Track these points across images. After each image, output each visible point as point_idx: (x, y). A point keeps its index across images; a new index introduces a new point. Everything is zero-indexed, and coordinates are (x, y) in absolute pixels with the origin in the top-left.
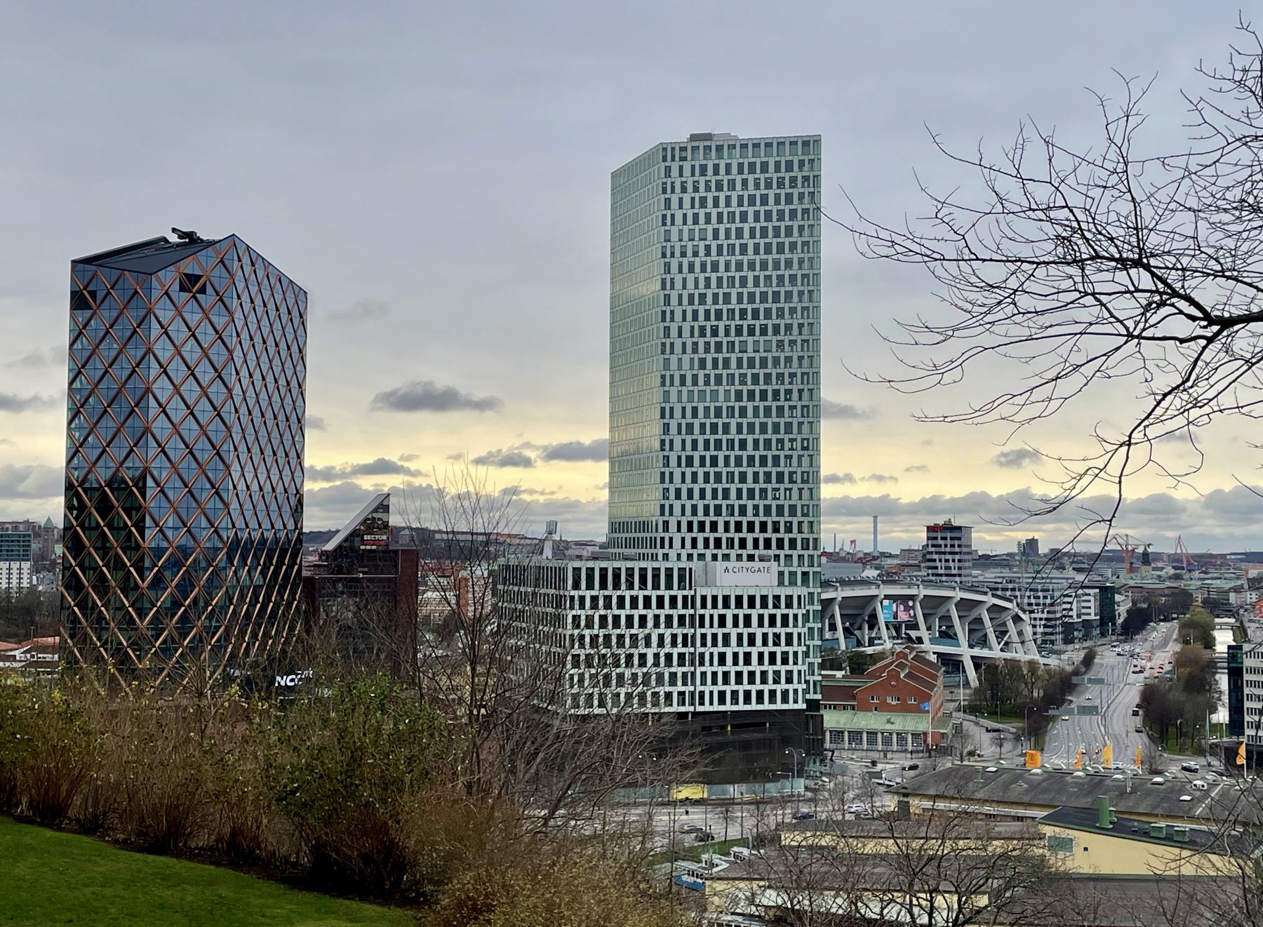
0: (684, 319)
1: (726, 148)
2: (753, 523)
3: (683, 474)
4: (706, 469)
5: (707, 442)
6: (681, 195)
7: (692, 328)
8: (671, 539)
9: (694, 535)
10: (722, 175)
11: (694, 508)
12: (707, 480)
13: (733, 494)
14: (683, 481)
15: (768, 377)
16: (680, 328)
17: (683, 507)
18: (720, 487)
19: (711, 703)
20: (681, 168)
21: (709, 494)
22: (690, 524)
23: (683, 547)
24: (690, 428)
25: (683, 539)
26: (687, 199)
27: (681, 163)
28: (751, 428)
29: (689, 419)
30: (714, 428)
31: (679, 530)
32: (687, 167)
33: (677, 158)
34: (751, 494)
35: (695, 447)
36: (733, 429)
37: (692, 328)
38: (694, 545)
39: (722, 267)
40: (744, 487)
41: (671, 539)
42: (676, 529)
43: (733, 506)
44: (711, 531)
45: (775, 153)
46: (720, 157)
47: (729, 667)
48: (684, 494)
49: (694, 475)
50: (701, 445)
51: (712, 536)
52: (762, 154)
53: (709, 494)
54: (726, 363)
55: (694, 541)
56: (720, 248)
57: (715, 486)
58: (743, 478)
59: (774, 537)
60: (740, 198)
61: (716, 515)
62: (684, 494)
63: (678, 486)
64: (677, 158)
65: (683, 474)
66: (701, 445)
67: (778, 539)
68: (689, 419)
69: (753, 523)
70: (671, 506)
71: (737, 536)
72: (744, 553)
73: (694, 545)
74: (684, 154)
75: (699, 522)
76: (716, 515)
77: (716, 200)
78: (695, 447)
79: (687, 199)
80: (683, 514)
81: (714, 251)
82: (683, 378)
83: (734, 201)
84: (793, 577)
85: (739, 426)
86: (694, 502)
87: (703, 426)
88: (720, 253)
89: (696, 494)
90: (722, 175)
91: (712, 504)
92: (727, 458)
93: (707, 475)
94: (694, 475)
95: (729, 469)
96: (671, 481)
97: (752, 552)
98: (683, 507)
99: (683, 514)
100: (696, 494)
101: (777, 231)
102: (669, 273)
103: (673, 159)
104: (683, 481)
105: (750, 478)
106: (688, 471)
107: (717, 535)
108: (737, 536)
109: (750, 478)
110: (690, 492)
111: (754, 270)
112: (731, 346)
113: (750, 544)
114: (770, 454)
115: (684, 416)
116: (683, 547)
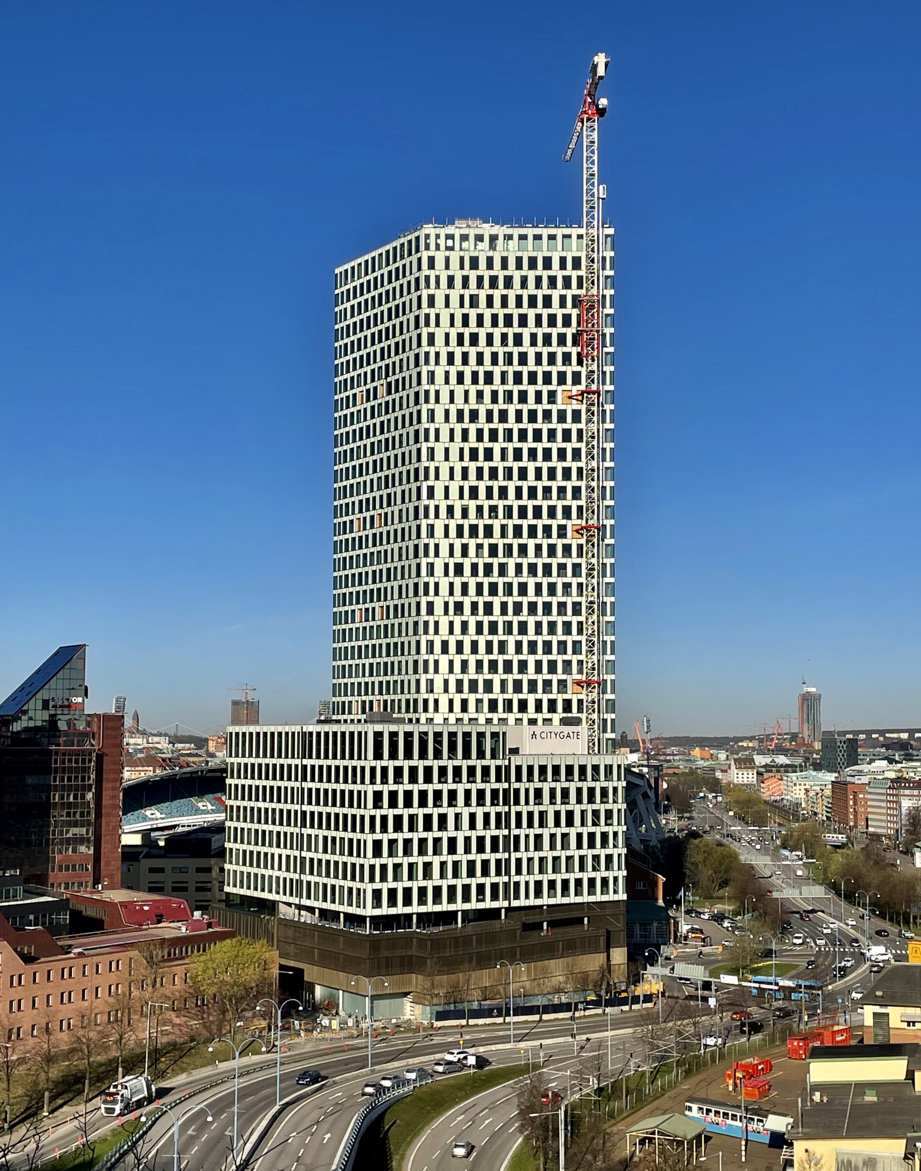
0: (452, 478)
1: (501, 238)
2: (535, 373)
3: (451, 624)
4: (479, 580)
5: (479, 586)
6: (447, 292)
7: (462, 450)
8: (437, 469)
9: (465, 426)
10: (497, 270)
11: (464, 664)
12: (479, 631)
13: (511, 493)
14: (451, 632)
15: (552, 434)
16: (447, 489)
17: (451, 663)
18: (495, 639)
19: (527, 896)
20: (447, 259)
21: (482, 647)
22: (459, 683)
23: (452, 325)
24: (459, 607)
25: (451, 702)
26: (454, 296)
27: (447, 253)
28: (533, 569)
29: (458, 597)
30: (488, 569)
31: (447, 535)
32: (454, 257)
33: (442, 247)
34: (533, 569)
35: (465, 591)
36: (511, 648)
37: (462, 450)
38: (464, 708)
39: (497, 378)
40: (525, 639)
41: (437, 469)
42: (443, 458)
43: (511, 662)
44: (485, 460)
45: (560, 247)
46: (492, 247)
47: (461, 856)
48: (452, 648)
49: (465, 625)
50: (472, 590)
51: (486, 465)
52: (545, 247)
53: (482, 647)
54: (503, 492)
55: (464, 703)
56: (495, 356)
57: (490, 483)
58: (523, 550)
59: (560, 466)
60: (519, 299)
61: (491, 440)
62: (452, 648)
63: (445, 638)
64: (442, 247)
65: (451, 624)
66: (472, 590)
67: (564, 316)
68: (458, 597)
69: (535, 373)
70: (436, 662)
71: (516, 466)
72: (525, 717)
73: (464, 708)
74: (450, 243)
75: (470, 681)
76: (491, 440)
77: (490, 299)
78: (465, 591)
79: (454, 296)
80: (451, 671)
81: (487, 359)
82: (451, 279)
83: (512, 301)
84: (578, 607)
85: (519, 645)
86: (464, 657)
87: (474, 567)
88: (495, 362)
89: (467, 648)
90: (497, 270)
91: (486, 659)
92: (503, 683)
93: (479, 625)
94: (465, 625)
95: (506, 618)
96: (436, 632)
97: (534, 716)
98: (451, 663)
99: (451, 671)
100: (467, 648)
101: (562, 454)
102: (432, 691)
103: (438, 247)
104: (451, 632)
105: (531, 474)
106: (458, 581)
107: (492, 464)
108: (516, 389)
109: (531, 397)
110: (460, 645)
111: (535, 460)
112: (509, 549)
113: (531, 706)
114: (554, 678)
115: (451, 555)
116: (452, 325)
